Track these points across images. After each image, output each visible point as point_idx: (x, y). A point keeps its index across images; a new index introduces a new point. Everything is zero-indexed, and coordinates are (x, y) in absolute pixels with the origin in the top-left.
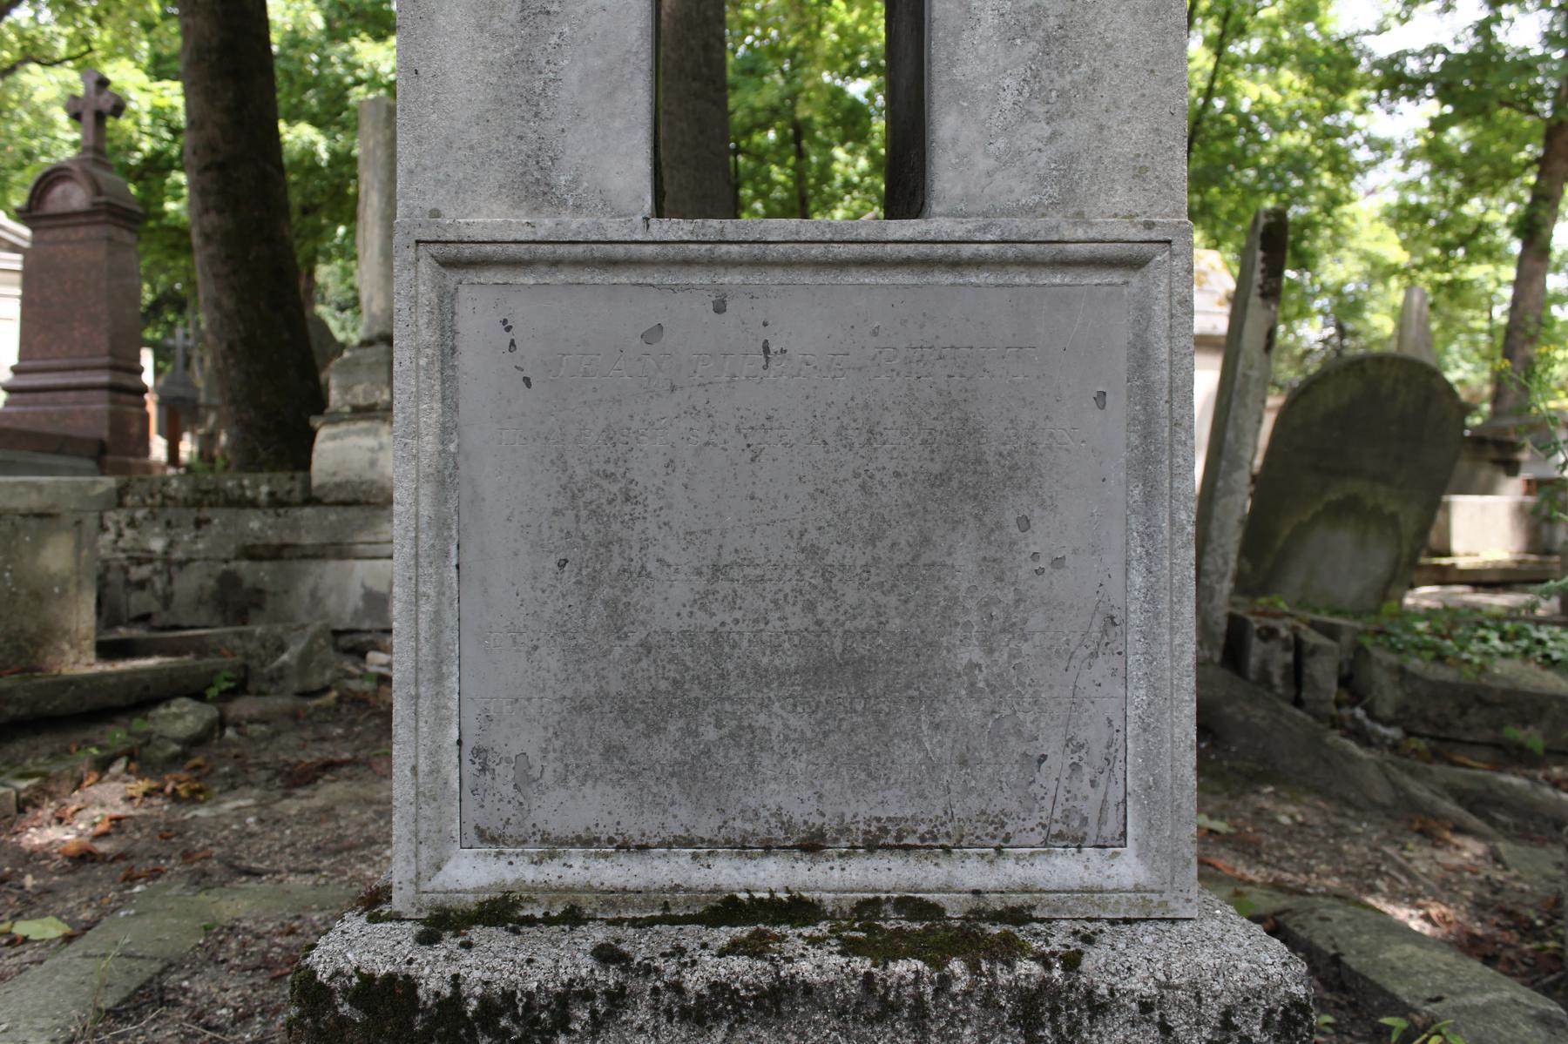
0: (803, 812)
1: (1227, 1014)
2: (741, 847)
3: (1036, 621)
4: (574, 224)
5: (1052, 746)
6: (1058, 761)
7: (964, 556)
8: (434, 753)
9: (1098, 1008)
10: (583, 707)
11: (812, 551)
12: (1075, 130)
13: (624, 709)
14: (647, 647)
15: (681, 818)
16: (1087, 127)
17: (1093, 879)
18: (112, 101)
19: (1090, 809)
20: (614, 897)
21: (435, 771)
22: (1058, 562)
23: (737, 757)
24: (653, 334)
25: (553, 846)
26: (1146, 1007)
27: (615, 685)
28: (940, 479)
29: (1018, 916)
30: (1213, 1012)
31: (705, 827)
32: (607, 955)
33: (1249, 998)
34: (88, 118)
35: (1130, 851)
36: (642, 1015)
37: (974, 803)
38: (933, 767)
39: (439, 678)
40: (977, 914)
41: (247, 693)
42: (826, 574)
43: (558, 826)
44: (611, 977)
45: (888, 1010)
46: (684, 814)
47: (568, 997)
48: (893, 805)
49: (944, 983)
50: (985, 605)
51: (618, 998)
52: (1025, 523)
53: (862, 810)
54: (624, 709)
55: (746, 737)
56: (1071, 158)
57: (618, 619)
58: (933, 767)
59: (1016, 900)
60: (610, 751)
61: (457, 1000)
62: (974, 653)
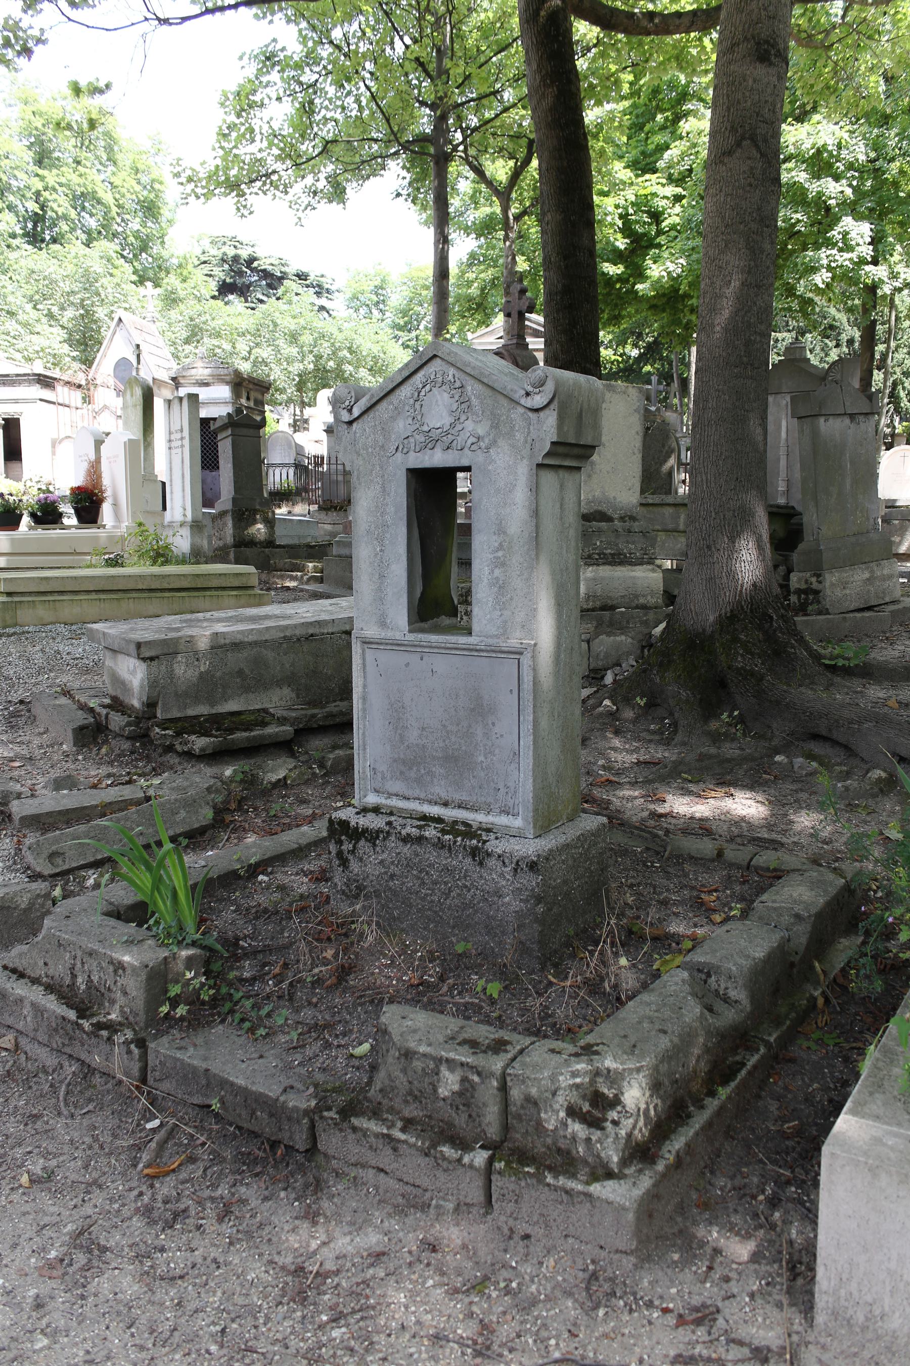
0: (444, 795)
1: (518, 862)
2: (430, 802)
3: (497, 751)
4: (389, 634)
5: (501, 786)
6: (503, 791)
7: (479, 731)
8: (364, 767)
9: (489, 855)
10: (395, 761)
11: (444, 726)
12: (507, 613)
13: (404, 762)
14: (408, 747)
15: (417, 793)
16: (510, 613)
17: (509, 824)
18: (527, 304)
19: (511, 804)
20: (401, 810)
21: (364, 772)
22: (502, 736)
23: (429, 779)
24: (407, 665)
25: (390, 795)
26: (499, 856)
27: (402, 756)
28: (473, 710)
29: (489, 830)
30: (515, 861)
31: (422, 796)
32: (389, 823)
33: (523, 858)
34: (515, 315)
35: (520, 818)
36: (393, 838)
37: (483, 799)
38: (474, 788)
39: (365, 749)
40: (480, 829)
41: (292, 754)
42: (447, 732)
43: (392, 790)
44: (387, 828)
45: (443, 847)
46: (418, 791)
47: (379, 831)
48: (464, 796)
49: (455, 842)
50: (485, 745)
51: (388, 833)
52: (493, 724)
53: (458, 796)
54: (404, 762)
55: (430, 773)
56: (506, 622)
57: (402, 738)
58: (474, 788)
59: (489, 826)
60: (402, 773)
61: (357, 828)
62: (481, 758)
